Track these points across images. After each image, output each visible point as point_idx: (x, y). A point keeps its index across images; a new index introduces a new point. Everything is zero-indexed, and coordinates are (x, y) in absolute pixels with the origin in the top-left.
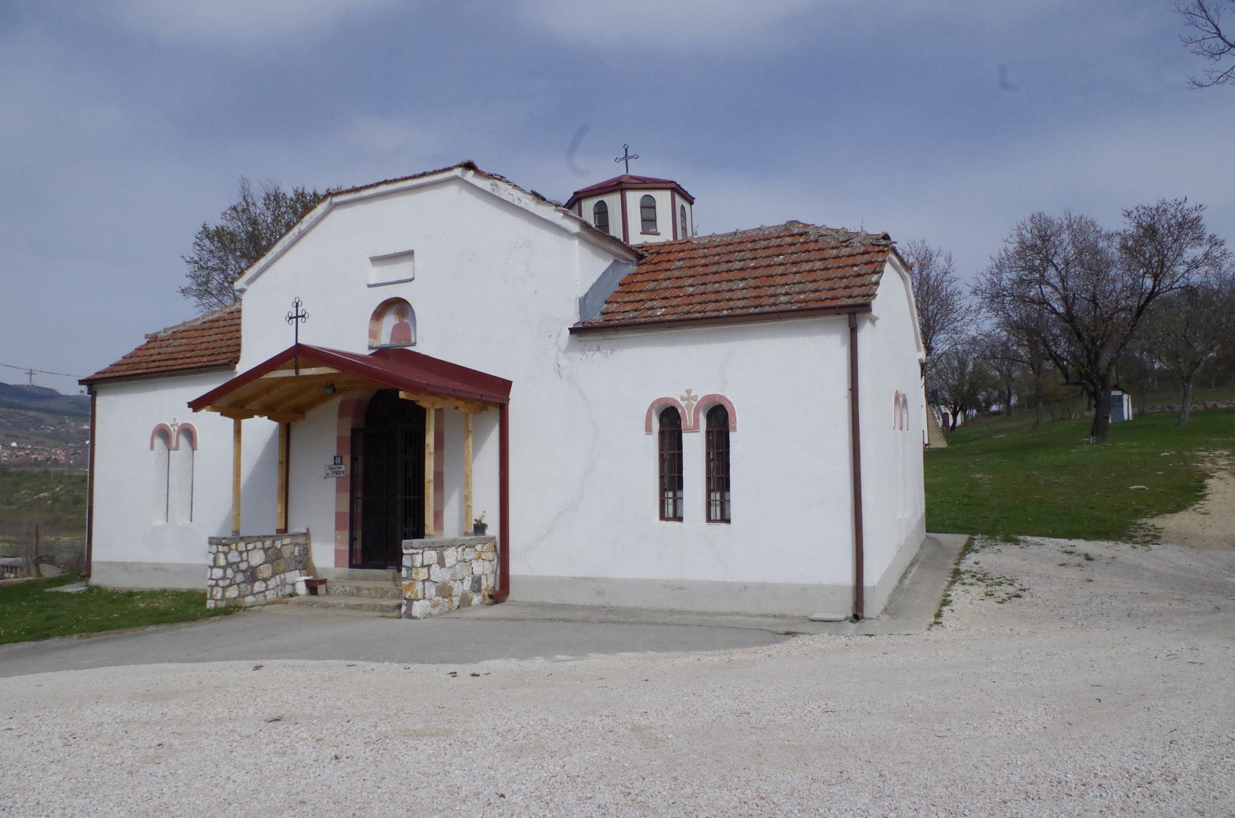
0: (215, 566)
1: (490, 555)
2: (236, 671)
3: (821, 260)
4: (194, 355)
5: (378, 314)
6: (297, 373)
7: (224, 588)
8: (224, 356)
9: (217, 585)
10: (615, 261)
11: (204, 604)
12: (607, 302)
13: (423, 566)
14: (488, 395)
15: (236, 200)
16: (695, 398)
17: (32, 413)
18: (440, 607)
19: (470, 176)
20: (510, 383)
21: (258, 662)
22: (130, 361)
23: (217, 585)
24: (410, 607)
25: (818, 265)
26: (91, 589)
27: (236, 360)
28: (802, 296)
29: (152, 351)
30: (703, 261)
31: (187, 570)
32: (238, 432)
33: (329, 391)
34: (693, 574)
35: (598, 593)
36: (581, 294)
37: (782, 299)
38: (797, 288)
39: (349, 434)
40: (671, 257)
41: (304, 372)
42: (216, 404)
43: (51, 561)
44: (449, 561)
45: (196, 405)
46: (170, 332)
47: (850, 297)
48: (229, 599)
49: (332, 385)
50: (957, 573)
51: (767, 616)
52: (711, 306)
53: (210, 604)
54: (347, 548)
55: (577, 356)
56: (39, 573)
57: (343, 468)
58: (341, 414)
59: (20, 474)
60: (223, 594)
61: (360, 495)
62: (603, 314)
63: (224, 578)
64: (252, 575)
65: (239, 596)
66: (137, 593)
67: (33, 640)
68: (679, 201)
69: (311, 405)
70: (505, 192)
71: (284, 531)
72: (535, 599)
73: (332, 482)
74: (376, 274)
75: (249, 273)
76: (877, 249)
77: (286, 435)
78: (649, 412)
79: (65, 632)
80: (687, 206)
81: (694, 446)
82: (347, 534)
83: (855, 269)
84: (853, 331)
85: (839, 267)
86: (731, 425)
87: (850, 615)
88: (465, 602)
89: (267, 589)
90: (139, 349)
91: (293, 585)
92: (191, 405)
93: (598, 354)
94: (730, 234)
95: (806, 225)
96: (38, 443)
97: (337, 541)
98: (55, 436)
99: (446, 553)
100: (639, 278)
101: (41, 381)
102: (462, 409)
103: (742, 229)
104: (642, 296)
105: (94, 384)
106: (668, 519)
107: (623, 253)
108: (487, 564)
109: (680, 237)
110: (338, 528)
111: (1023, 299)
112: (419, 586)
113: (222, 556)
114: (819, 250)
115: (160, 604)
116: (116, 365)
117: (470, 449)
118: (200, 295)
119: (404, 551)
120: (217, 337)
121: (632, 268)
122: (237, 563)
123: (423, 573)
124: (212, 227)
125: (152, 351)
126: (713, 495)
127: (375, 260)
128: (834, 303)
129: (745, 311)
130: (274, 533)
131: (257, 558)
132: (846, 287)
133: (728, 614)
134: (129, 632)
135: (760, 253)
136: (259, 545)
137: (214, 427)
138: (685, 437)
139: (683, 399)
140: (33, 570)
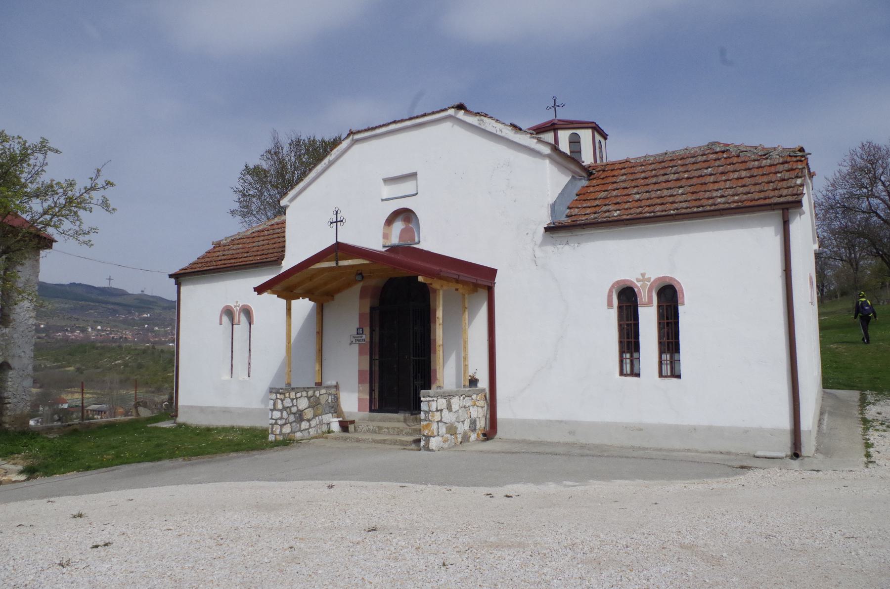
0: (275, 409)
1: (482, 403)
2: (316, 488)
3: (745, 170)
4: (250, 254)
5: (390, 221)
6: (337, 264)
7: (282, 426)
8: (272, 255)
9: (276, 423)
10: (573, 177)
11: (266, 437)
12: (569, 208)
13: (437, 411)
14: (479, 280)
15: (270, 146)
17: (110, 307)
19: (461, 114)
20: (495, 271)
21: (404, 485)
22: (203, 261)
23: (276, 423)
24: (427, 442)
25: (744, 174)
26: (180, 425)
27: (282, 258)
28: (736, 198)
29: (218, 254)
30: (643, 175)
31: (247, 413)
32: (289, 309)
33: (359, 278)
34: (649, 419)
35: (570, 433)
36: (551, 201)
37: (719, 200)
38: (730, 192)
39: (368, 311)
40: (615, 173)
41: (343, 263)
42: (274, 289)
43: (145, 405)
44: (455, 407)
45: (260, 290)
46: (229, 240)
47: (781, 196)
48: (284, 435)
49: (361, 274)
50: (865, 421)
51: (715, 453)
52: (658, 208)
53: (271, 438)
54: (368, 397)
55: (549, 248)
56: (138, 414)
57: (364, 337)
58: (363, 295)
59: (103, 348)
60: (281, 430)
61: (377, 357)
62: (567, 216)
63: (281, 418)
64: (300, 416)
65: (291, 432)
66: (213, 429)
67: (151, 461)
68: (598, 137)
69: (339, 290)
70: (489, 125)
71: (319, 385)
72: (517, 437)
73: (356, 348)
74: (387, 191)
75: (291, 194)
76: (795, 159)
77: (320, 311)
78: (611, 291)
79: (172, 456)
80: (602, 141)
82: (367, 386)
83: (779, 175)
84: (786, 224)
85: (763, 175)
86: (680, 301)
87: (789, 453)
89: (310, 427)
90: (209, 252)
91: (328, 424)
92: (256, 289)
93: (567, 247)
94: (662, 155)
95: (728, 145)
96: (115, 327)
97: (359, 391)
98: (125, 322)
99: (452, 401)
100: (592, 189)
101: (115, 285)
102: (461, 291)
103: (670, 150)
104: (597, 202)
105: (179, 278)
106: (626, 375)
107: (578, 170)
108: (480, 409)
109: (598, 161)
110: (361, 381)
111: (847, 210)
112: (434, 426)
113: (279, 401)
114: (742, 162)
115: (236, 437)
116: (193, 264)
117: (467, 321)
118: (244, 215)
119: (422, 399)
120: (264, 243)
121: (584, 183)
123: (437, 416)
124: (252, 167)
125: (218, 254)
126: (664, 356)
127: (388, 181)
128: (767, 201)
129: (689, 210)
130: (313, 385)
132: (774, 190)
133: (679, 451)
134: (218, 457)
135: (690, 167)
136: (304, 394)
137: (271, 306)
138: (641, 310)
139: (638, 280)
140: (134, 411)
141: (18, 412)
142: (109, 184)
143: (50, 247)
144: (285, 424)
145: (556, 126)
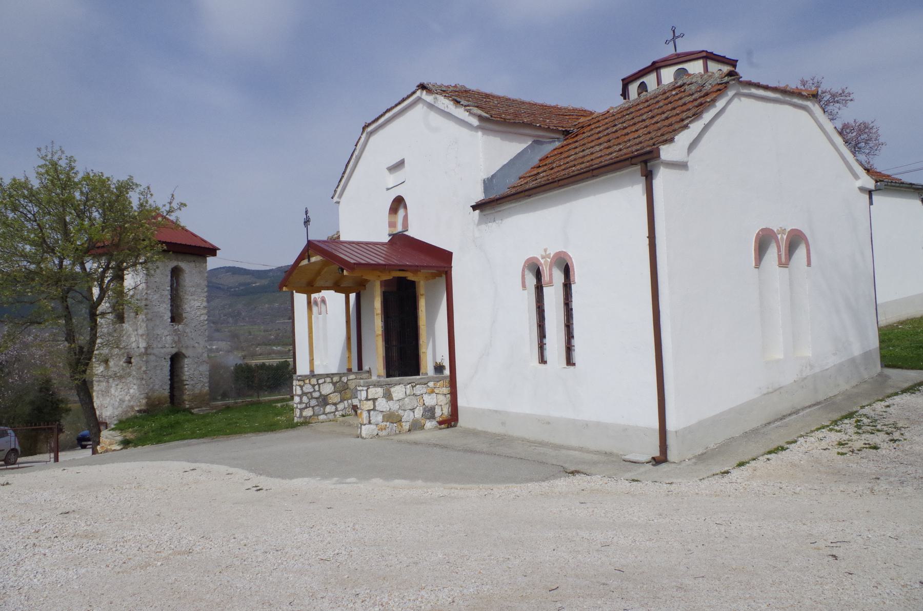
10: (534, 141)
16: (548, 256)
18: (387, 430)
34: (528, 412)
48: (306, 418)
60: (301, 413)
64: (324, 401)
81: (553, 296)
88: (416, 426)
108: (441, 397)
122: (311, 393)
131: (327, 389)
133: (574, 449)
136: (328, 380)
141: (197, 391)
142: (184, 205)
143: (214, 254)
144: (306, 407)
145: (657, 65)
